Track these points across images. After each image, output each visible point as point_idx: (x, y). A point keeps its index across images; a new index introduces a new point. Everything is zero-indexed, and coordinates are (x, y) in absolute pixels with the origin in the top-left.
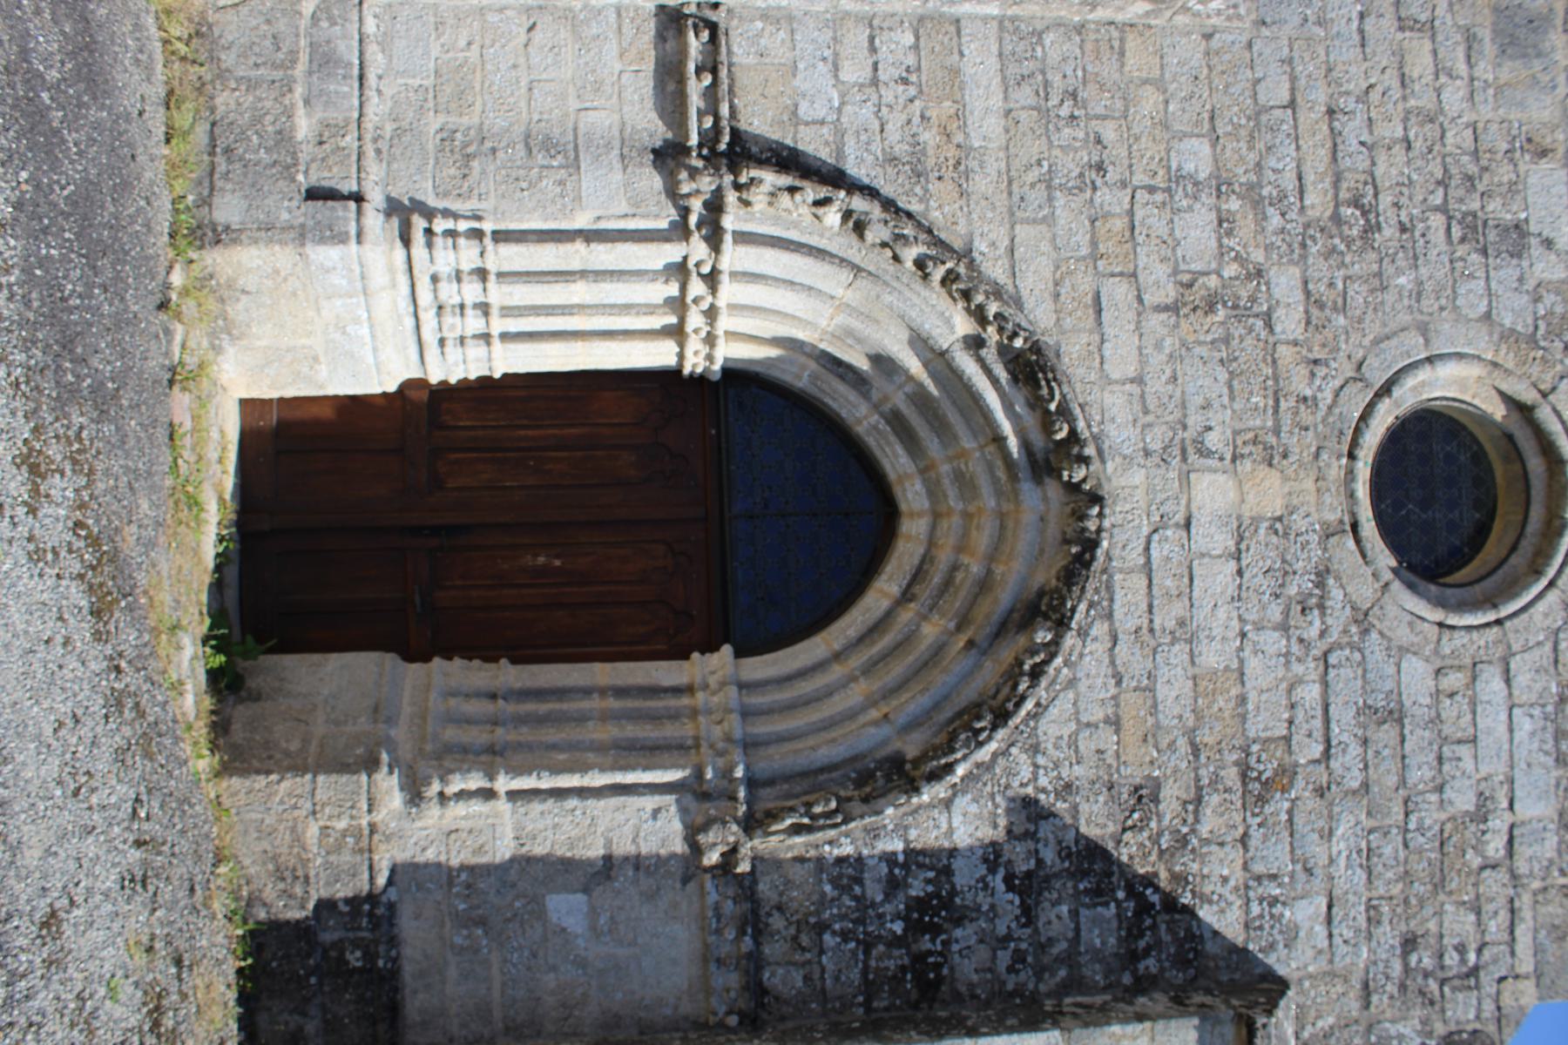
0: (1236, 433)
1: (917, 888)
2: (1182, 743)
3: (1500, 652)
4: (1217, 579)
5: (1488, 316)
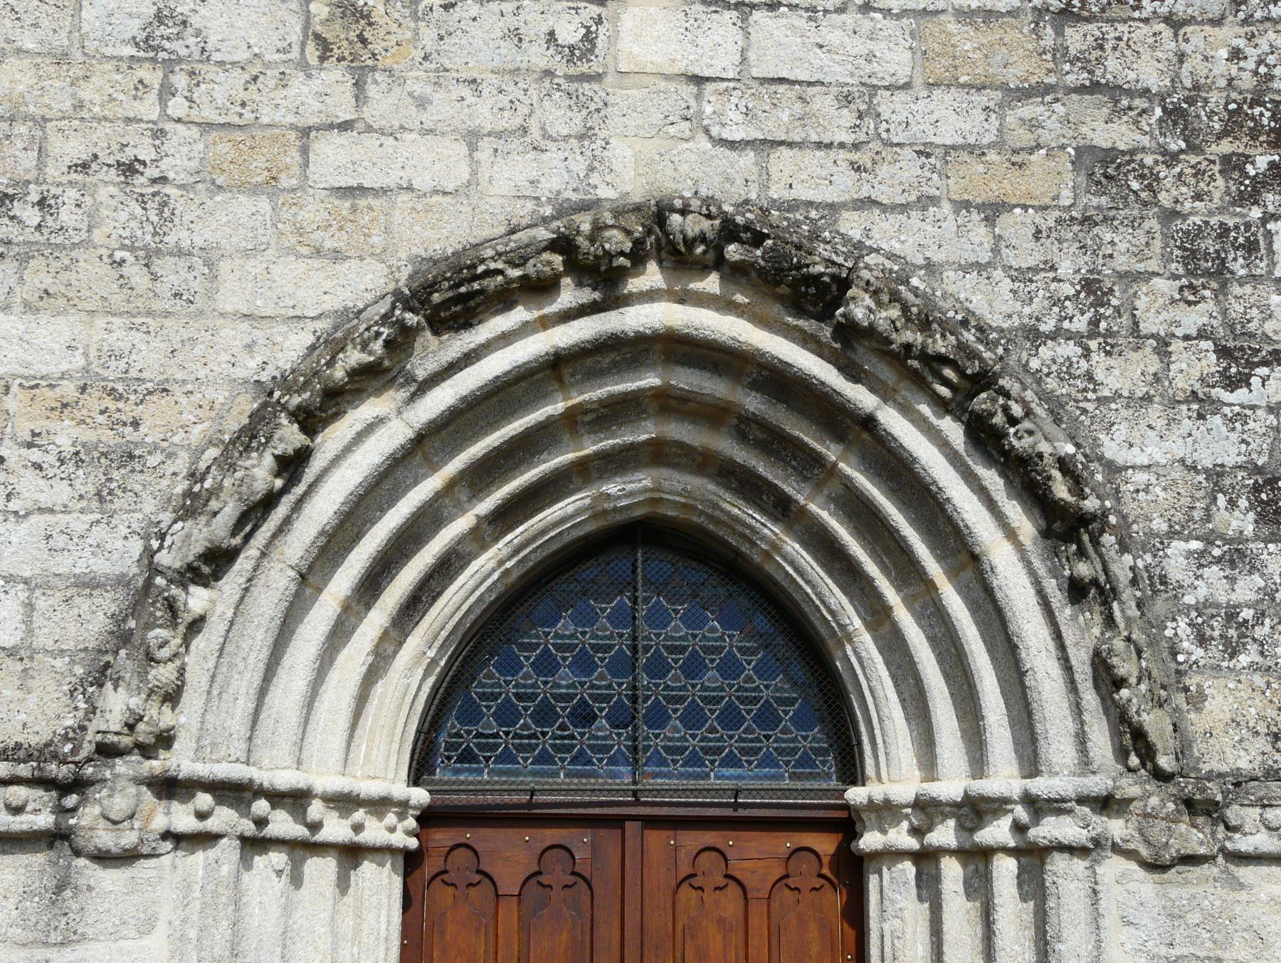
1: (1242, 522)
2: (1029, 110)
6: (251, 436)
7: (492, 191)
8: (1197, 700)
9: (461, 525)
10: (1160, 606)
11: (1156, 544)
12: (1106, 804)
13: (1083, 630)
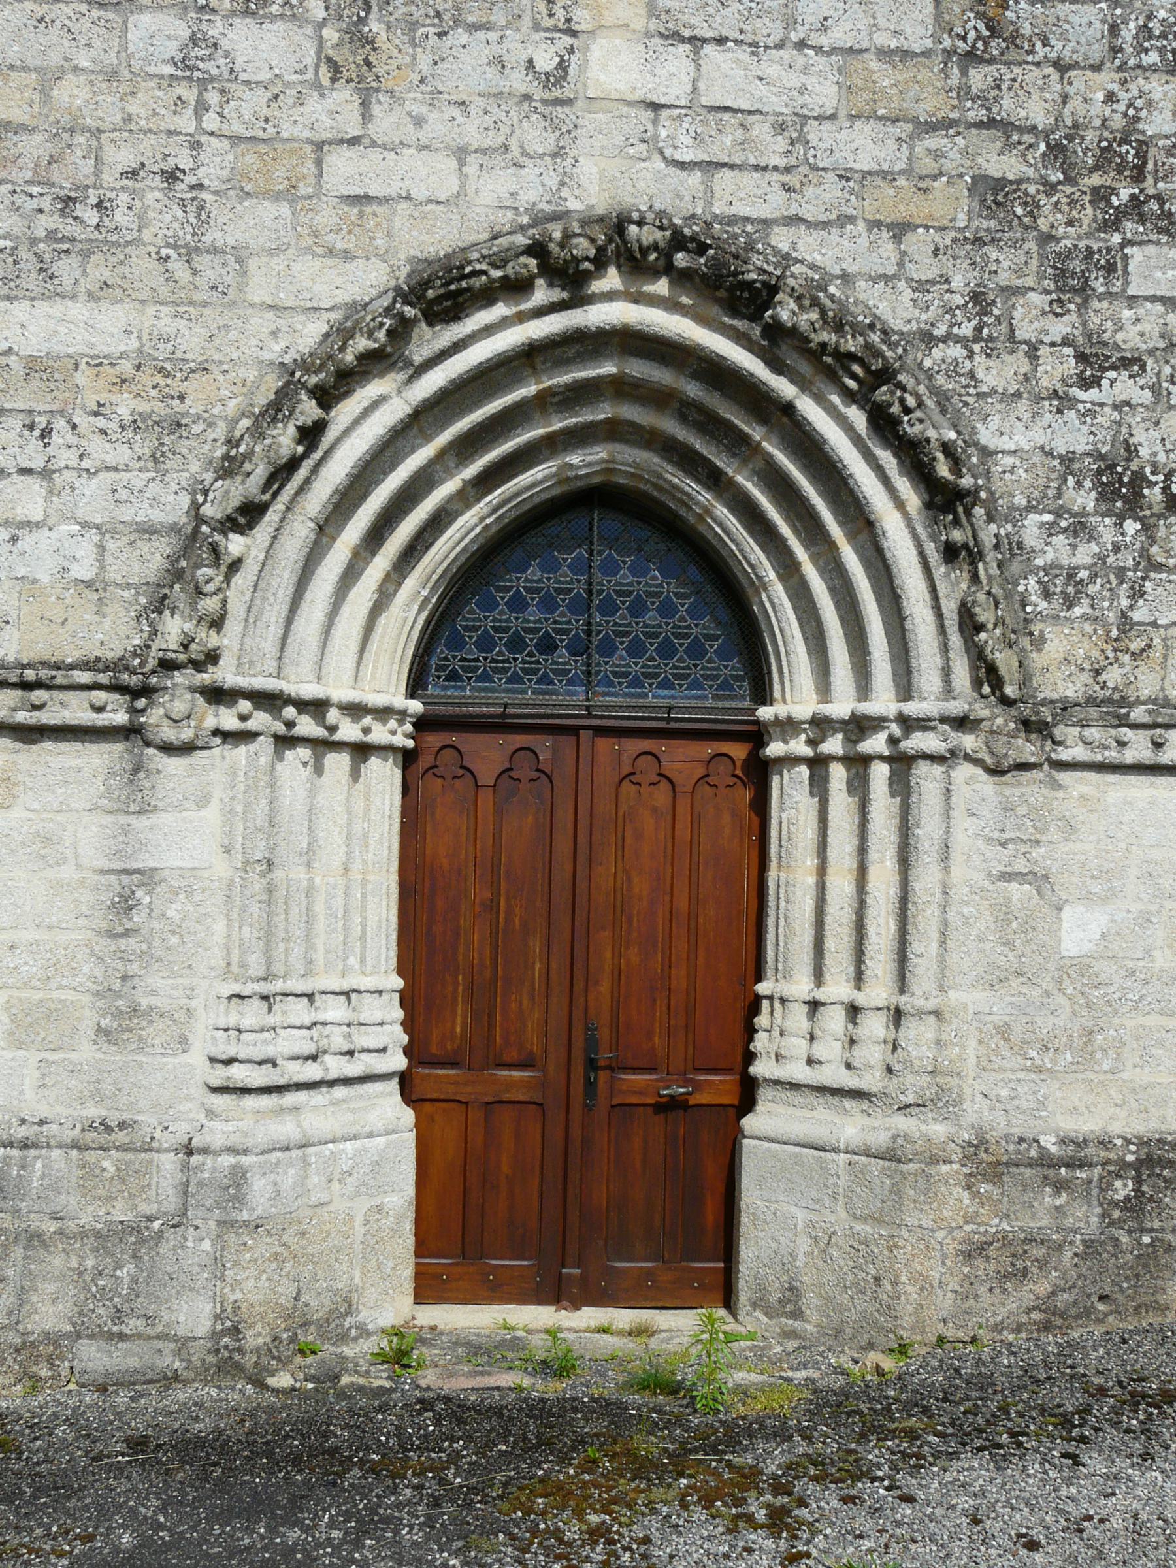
0: (537, 27)
1: (1085, 499)
2: (935, 141)
4: (727, 75)
6: (277, 409)
7: (478, 201)
8: (1039, 643)
10: (1015, 567)
11: (1015, 516)
12: (962, 723)
13: (953, 586)
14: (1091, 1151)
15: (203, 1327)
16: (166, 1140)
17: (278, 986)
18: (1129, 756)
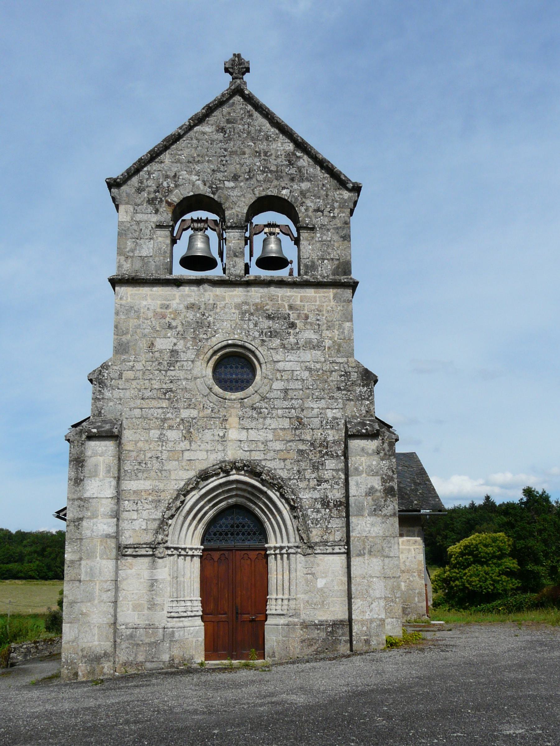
0: (220, 428)
1: (319, 506)
2: (290, 444)
3: (272, 363)
4: (253, 435)
5: (193, 361)
6: (176, 498)
8: (311, 532)
9: (207, 508)
10: (307, 519)
11: (306, 510)
12: (298, 547)
13: (296, 522)
14: (324, 623)
15: (168, 659)
16: (160, 627)
17: (179, 599)
18: (328, 552)
